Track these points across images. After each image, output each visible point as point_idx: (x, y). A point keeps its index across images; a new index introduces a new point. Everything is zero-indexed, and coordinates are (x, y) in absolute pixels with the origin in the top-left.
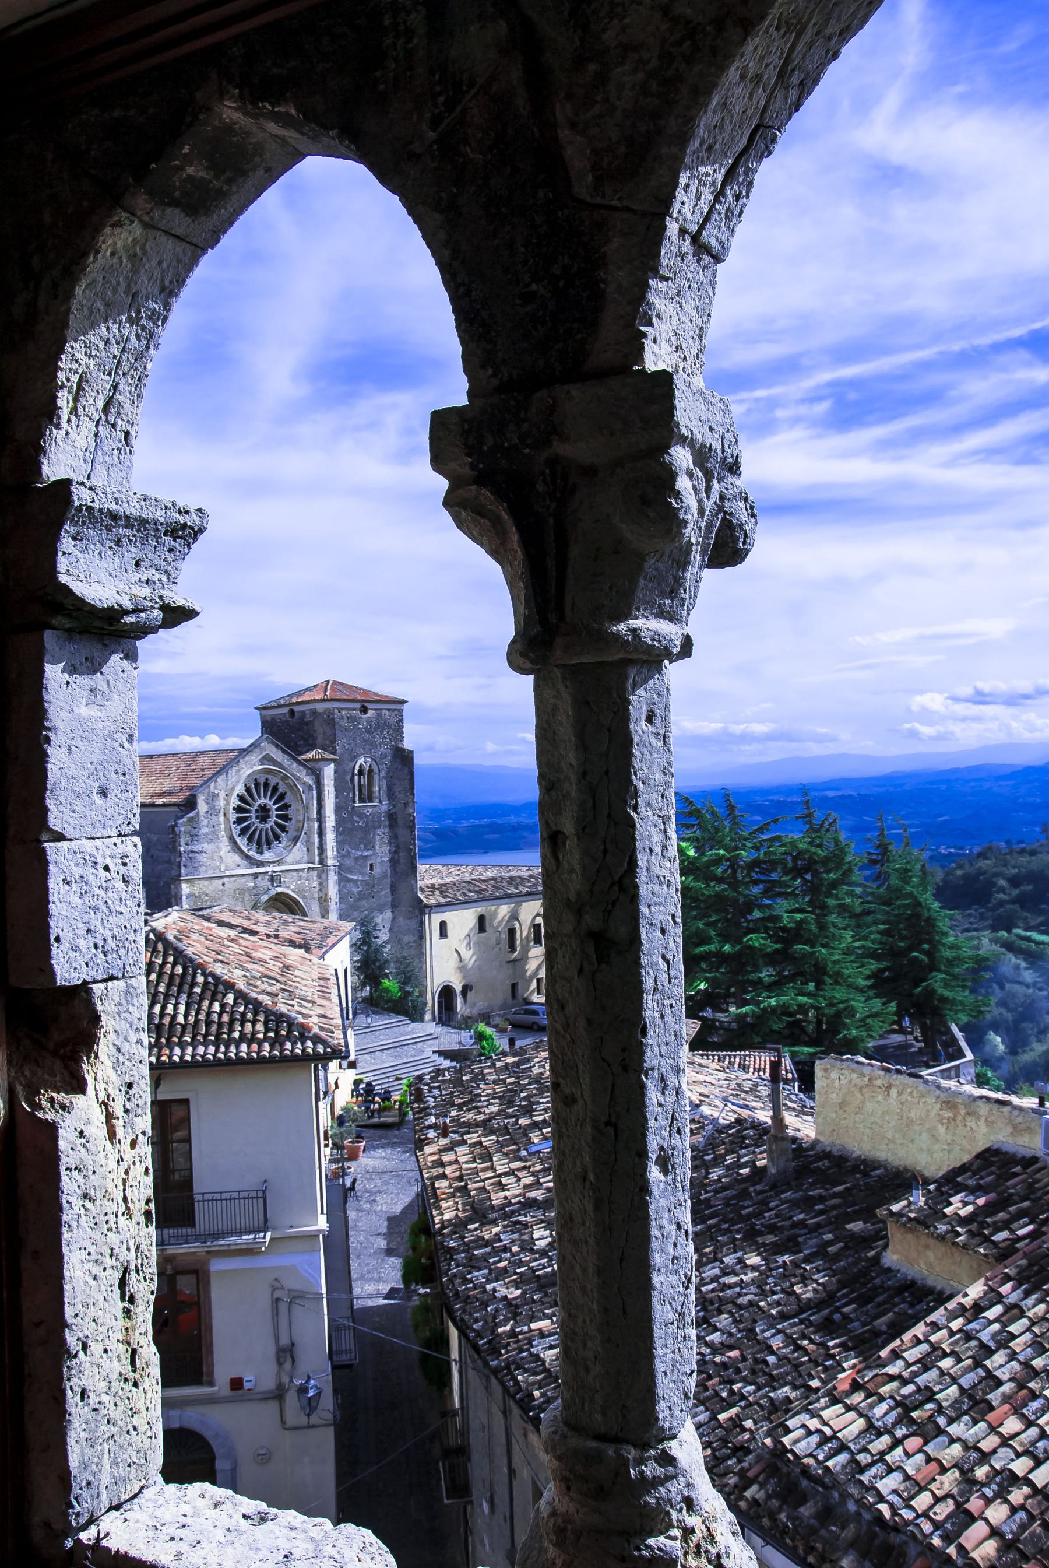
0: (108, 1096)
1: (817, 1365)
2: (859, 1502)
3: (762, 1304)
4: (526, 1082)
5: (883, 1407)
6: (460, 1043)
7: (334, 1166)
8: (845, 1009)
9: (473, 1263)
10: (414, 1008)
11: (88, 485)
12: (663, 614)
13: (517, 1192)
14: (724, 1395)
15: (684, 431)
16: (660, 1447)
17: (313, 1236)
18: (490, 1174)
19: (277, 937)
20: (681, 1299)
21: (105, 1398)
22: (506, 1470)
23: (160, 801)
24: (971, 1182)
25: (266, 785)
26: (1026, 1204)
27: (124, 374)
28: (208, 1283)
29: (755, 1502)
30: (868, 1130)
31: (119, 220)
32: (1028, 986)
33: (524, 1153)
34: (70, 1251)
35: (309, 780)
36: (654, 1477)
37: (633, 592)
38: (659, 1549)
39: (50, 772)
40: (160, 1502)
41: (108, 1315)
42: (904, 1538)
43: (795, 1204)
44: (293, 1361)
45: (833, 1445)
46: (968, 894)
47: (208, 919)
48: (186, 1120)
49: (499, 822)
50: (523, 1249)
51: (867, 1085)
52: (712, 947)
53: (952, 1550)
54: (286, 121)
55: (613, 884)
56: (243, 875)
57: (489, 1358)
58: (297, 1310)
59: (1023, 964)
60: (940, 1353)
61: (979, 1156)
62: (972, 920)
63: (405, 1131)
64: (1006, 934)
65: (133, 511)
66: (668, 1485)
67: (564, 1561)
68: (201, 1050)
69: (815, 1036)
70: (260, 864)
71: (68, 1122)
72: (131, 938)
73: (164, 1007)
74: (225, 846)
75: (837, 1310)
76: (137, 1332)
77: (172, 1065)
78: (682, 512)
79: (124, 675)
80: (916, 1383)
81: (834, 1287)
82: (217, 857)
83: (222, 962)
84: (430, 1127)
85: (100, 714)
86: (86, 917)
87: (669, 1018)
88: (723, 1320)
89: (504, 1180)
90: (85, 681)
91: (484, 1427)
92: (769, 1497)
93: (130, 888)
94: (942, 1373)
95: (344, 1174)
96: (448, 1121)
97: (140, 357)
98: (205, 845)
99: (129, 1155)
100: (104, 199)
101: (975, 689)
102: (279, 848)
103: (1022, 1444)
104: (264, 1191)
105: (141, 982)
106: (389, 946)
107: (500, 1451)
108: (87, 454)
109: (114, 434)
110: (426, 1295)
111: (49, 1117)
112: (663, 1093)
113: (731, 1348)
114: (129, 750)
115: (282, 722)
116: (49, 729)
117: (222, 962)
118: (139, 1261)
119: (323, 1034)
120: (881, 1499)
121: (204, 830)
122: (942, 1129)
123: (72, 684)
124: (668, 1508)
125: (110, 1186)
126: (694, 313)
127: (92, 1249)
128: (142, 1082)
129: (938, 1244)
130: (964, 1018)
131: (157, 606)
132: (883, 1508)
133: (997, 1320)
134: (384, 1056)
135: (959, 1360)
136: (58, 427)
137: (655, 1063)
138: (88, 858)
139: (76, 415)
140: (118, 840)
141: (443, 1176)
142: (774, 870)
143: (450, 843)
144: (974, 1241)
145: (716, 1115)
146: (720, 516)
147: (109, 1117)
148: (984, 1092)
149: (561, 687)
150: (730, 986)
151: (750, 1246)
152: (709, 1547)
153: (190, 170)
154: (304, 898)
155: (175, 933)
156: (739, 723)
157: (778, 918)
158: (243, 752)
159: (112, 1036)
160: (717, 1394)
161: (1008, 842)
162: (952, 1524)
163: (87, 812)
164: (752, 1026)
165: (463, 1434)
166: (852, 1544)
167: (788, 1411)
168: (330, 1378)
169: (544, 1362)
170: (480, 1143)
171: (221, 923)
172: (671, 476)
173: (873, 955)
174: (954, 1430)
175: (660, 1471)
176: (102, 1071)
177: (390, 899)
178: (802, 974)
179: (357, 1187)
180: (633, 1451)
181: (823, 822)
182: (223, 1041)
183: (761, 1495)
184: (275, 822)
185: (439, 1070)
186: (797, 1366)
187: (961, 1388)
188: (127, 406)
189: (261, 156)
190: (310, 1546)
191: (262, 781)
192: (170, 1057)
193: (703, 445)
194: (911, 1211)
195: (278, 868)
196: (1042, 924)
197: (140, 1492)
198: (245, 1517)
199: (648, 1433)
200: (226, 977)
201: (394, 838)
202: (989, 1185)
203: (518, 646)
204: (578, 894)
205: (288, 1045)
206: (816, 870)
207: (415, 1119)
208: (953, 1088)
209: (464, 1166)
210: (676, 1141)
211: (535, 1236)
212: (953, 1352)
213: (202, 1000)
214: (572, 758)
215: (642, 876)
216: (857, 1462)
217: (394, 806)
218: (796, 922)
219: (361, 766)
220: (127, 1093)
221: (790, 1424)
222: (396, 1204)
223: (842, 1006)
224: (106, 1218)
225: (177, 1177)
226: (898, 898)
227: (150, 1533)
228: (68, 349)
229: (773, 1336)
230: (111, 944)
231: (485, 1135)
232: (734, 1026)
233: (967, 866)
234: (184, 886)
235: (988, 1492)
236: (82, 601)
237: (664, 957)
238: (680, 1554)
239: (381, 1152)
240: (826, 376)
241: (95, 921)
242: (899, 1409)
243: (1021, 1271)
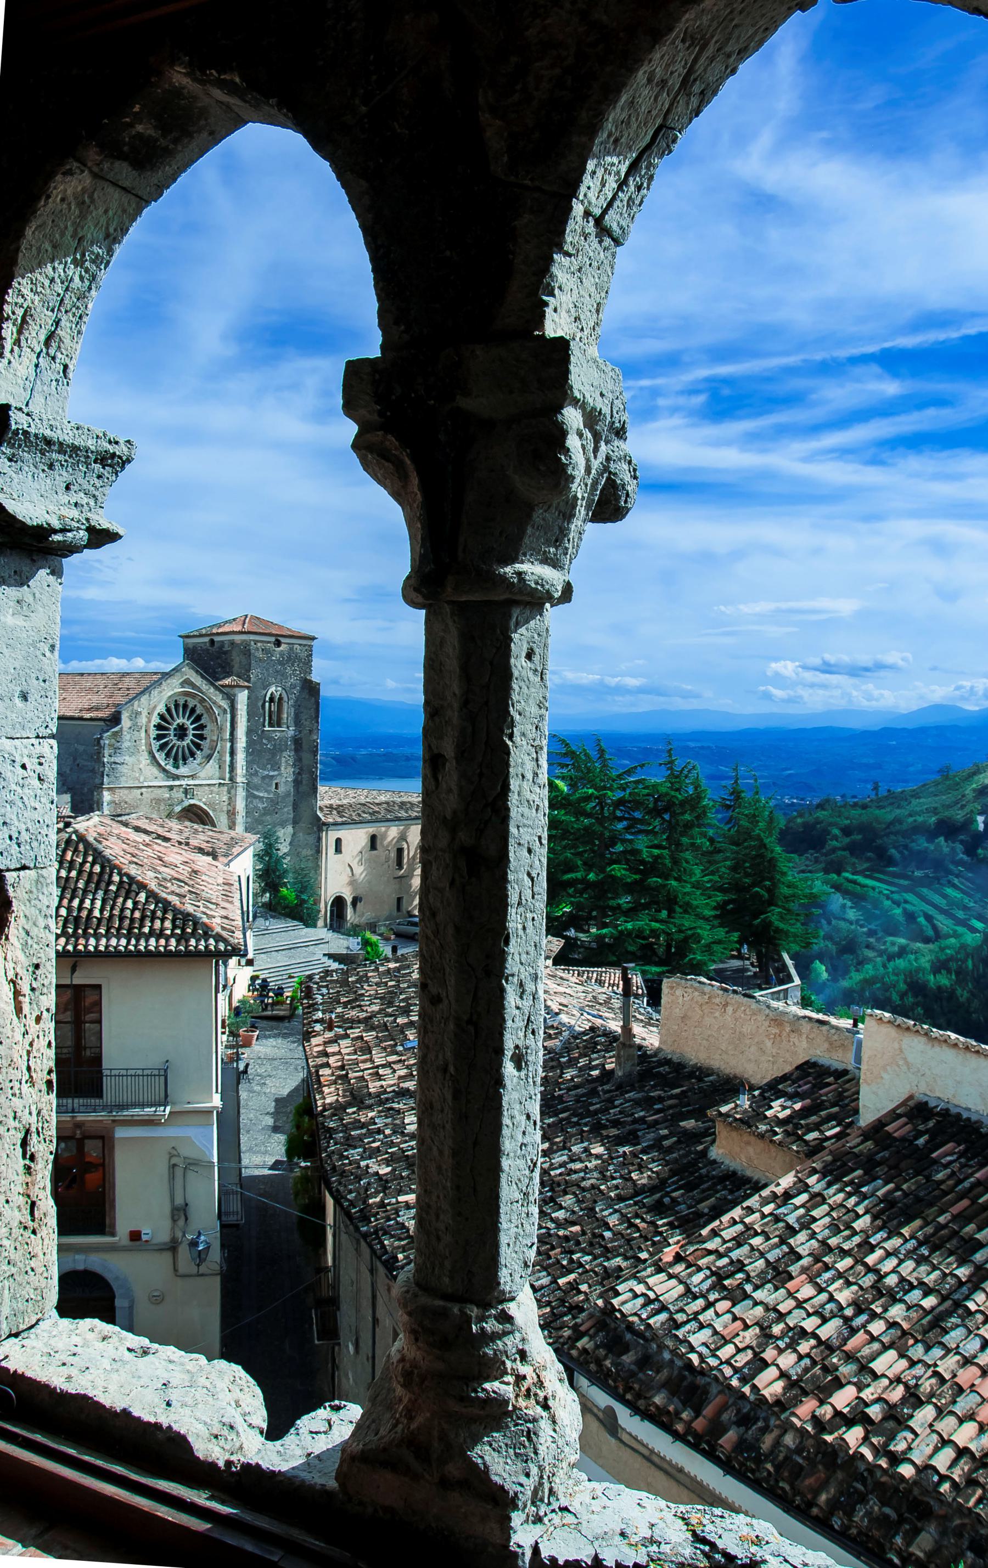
1: (646, 1239)
2: (674, 1352)
3: (602, 1187)
4: (406, 985)
5: (701, 1276)
7: (230, 1051)
9: (350, 1142)
11: (26, 410)
12: (547, 561)
13: (392, 1082)
14: (565, 1263)
15: (577, 394)
17: (209, 1112)
18: (368, 1065)
19: (187, 844)
23: (88, 716)
24: (790, 1090)
26: (836, 1109)
29: (585, 1351)
32: (851, 923)
33: (400, 1048)
35: (225, 704)
37: (521, 539)
43: (637, 1103)
44: (186, 1219)
45: (656, 1306)
47: (126, 824)
48: (99, 1003)
49: (395, 751)
52: (579, 875)
53: (747, 1390)
59: (849, 904)
61: (797, 1068)
63: (295, 1023)
65: (67, 438)
66: (505, 1339)
68: (114, 942)
70: (176, 777)
72: (44, 832)
74: (144, 759)
77: (87, 954)
78: (570, 468)
79: (49, 589)
81: (666, 1175)
82: (135, 767)
84: (317, 1021)
88: (568, 1200)
89: (381, 1071)
92: (597, 1347)
93: (45, 786)
95: (238, 1059)
97: (82, 297)
98: (127, 758)
103: (813, 1306)
104: (166, 1071)
105: (51, 873)
109: (53, 366)
110: (307, 1167)
112: (521, 998)
113: (574, 1223)
115: (202, 650)
119: (224, 934)
120: (692, 1349)
122: (769, 1044)
124: (504, 1358)
125: (16, 1057)
126: (593, 289)
128: (48, 964)
132: (694, 1358)
133: (803, 1206)
134: (279, 956)
135: (768, 1238)
137: (515, 970)
139: (19, 346)
140: (36, 741)
141: (327, 1065)
143: (348, 768)
144: (789, 1140)
145: (573, 1022)
147: (17, 993)
149: (450, 623)
150: (592, 910)
153: (140, 128)
154: (214, 810)
155: (95, 835)
156: (613, 676)
158: (166, 675)
159: (22, 921)
160: (558, 1262)
161: (843, 796)
163: (9, 714)
165: (334, 1288)
167: (618, 1277)
168: (218, 1235)
170: (361, 1038)
171: (137, 829)
172: (562, 434)
173: (721, 889)
174: (758, 1295)
175: (499, 1327)
178: (657, 903)
179: (249, 1071)
180: (475, 1310)
186: (629, 1241)
187: (767, 1261)
188: (67, 340)
191: (181, 702)
192: (86, 946)
193: (594, 409)
195: (191, 782)
201: (298, 761)
203: (412, 581)
204: (455, 812)
205: (193, 942)
210: (530, 1041)
211: (406, 1121)
212: (763, 1232)
213: (116, 897)
215: (513, 799)
216: (674, 1321)
221: (620, 1288)
223: (690, 932)
225: (88, 1053)
228: (15, 284)
230: (25, 836)
231: (366, 1031)
232: (594, 945)
233: (807, 815)
234: (106, 793)
235: (782, 1344)
236: (13, 518)
237: (529, 874)
241: (11, 815)
242: (714, 1278)
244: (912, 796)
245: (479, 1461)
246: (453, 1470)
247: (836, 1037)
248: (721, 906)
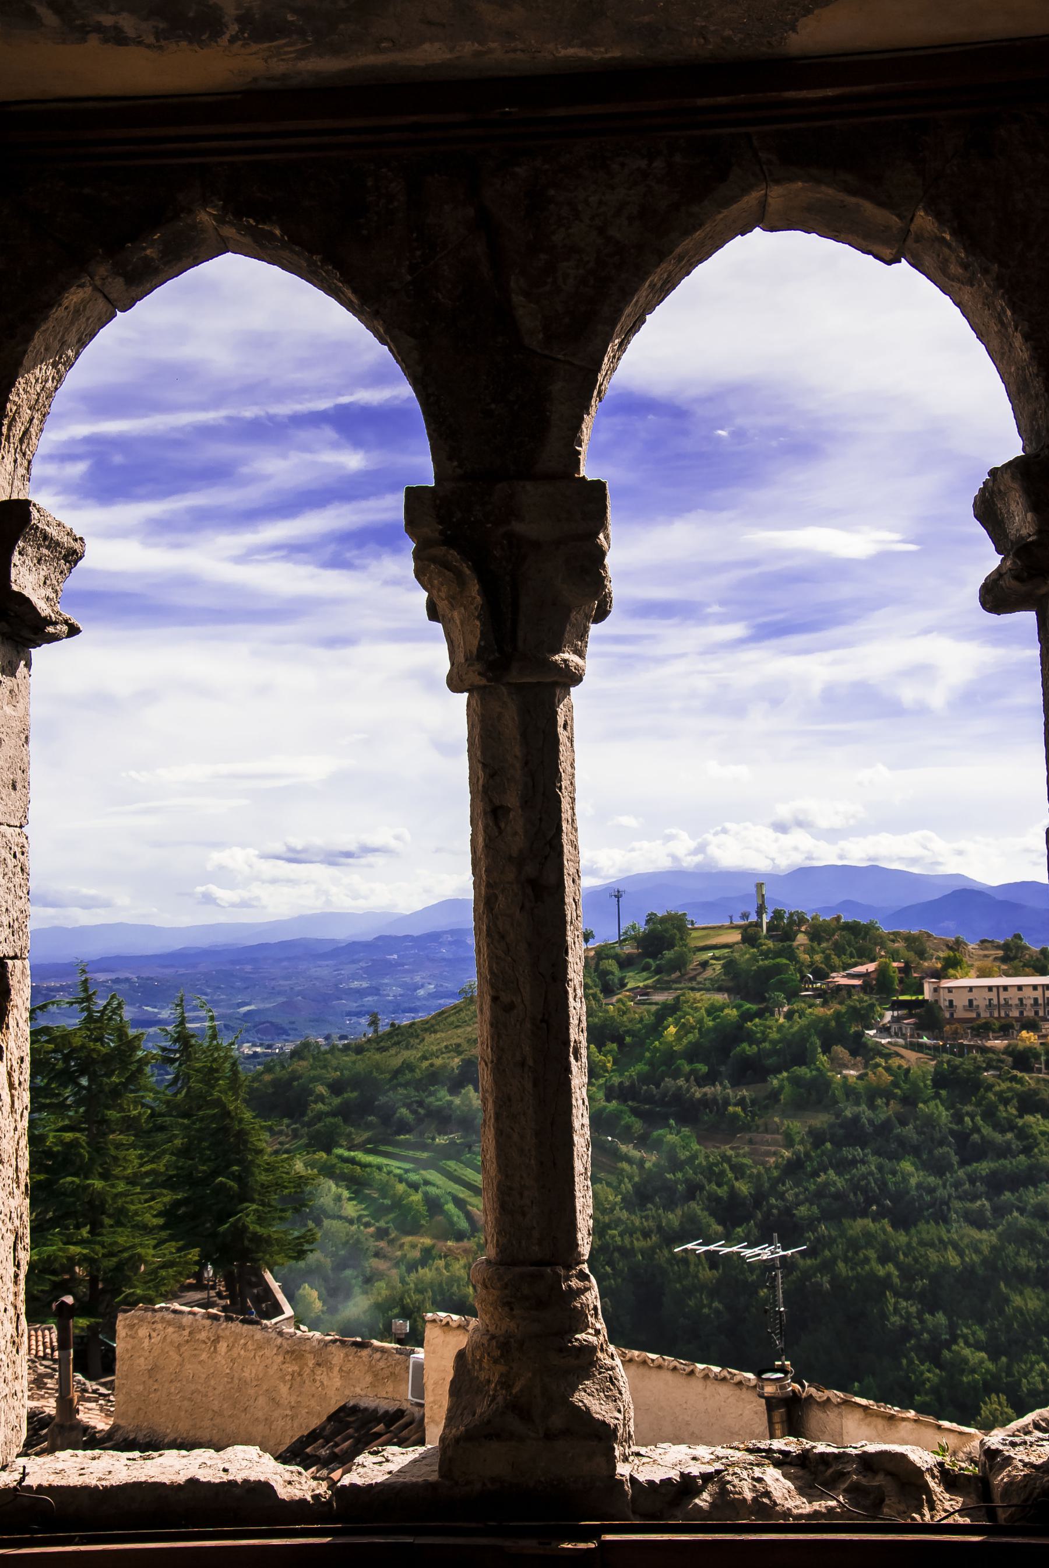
8: (131, 1257)
24: (323, 1452)
30: (186, 1403)
32: (351, 1222)
37: (563, 634)
51: (187, 1341)
59: (346, 1194)
61: (330, 1418)
62: (282, 1139)
64: (324, 1155)
69: (87, 1299)
101: (285, 844)
122: (284, 1389)
173: (169, 1183)
175: (581, 1284)
181: (105, 1007)
196: (369, 1141)
206: (95, 1071)
214: (517, 750)
223: (126, 1255)
226: (199, 1109)
240: (82, 430)
244: (426, 1030)
245: (581, 1404)
246: (557, 1422)
247: (382, 1364)
248: (169, 1214)
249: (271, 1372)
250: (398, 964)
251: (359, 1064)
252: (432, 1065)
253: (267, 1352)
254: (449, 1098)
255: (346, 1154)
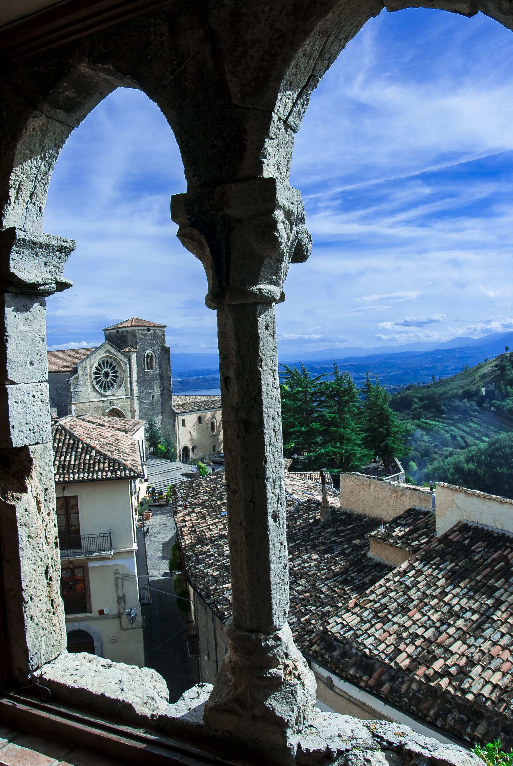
0: (37, 494)
1: (341, 597)
2: (357, 649)
3: (318, 574)
4: (220, 486)
5: (367, 612)
6: (191, 470)
7: (139, 523)
8: (353, 453)
10: (172, 456)
11: (23, 229)
12: (272, 283)
13: (216, 532)
14: (303, 611)
16: (274, 634)
17: (131, 552)
19: (113, 427)
20: (283, 574)
21: (41, 619)
22: (214, 643)
23: (62, 370)
24: (403, 522)
25: (107, 362)
26: (425, 530)
27: (39, 182)
28: (88, 571)
29: (315, 651)
31: (36, 115)
34: (23, 559)
35: (126, 360)
36: (272, 646)
38: (274, 673)
39: (8, 354)
40: (66, 660)
41: (40, 586)
42: (374, 661)
44: (125, 603)
45: (347, 628)
46: (402, 404)
47: (83, 420)
48: (76, 505)
49: (207, 377)
50: (219, 555)
52: (297, 429)
53: (392, 664)
54: (108, 72)
55: (251, 399)
56: (98, 401)
57: (206, 599)
58: (125, 582)
59: (425, 433)
60: (390, 590)
61: (406, 512)
63: (169, 507)
65: (43, 241)
66: (278, 648)
67: (235, 680)
68: (82, 475)
70: (106, 396)
71: (20, 505)
72: (45, 426)
73: (65, 458)
74: (90, 389)
75: (349, 575)
76: (54, 592)
77: (70, 482)
78: (280, 239)
80: (380, 603)
82: (86, 393)
83: (90, 438)
84: (179, 506)
85: (29, 329)
86: (25, 418)
87: (276, 456)
88: (303, 581)
89: (211, 527)
90: (23, 315)
91: (204, 627)
92: (321, 649)
94: (391, 598)
95: (144, 526)
96: (187, 503)
98: (82, 389)
99: (47, 518)
100: (30, 106)
101: (404, 319)
102: (113, 390)
103: (421, 623)
104: (110, 534)
106: (161, 430)
107: (211, 636)
108: (23, 216)
111: (12, 503)
112: (274, 488)
113: (306, 592)
114: (42, 345)
115: (113, 336)
116: (7, 336)
117: (90, 438)
118: (53, 563)
119: (133, 468)
120: (366, 647)
121: (81, 382)
122: (391, 501)
123: (17, 316)
124: (278, 657)
127: (33, 558)
129: (390, 547)
130: (401, 456)
131: (54, 282)
132: (367, 651)
133: (413, 576)
135: (397, 593)
136: (10, 204)
137: (270, 475)
138: (25, 392)
139: (18, 200)
140: (38, 384)
141: (186, 526)
142: (322, 396)
143: (186, 386)
145: (299, 498)
146: (296, 241)
147: (38, 503)
148: (408, 486)
150: (305, 445)
151: (313, 551)
152: (295, 672)
153: (67, 93)
154: (124, 410)
155: (69, 426)
157: (325, 416)
158: (97, 349)
159: (38, 468)
160: (300, 610)
161: (418, 383)
162: (393, 655)
163: (25, 372)
164: (314, 461)
165: (196, 630)
166: (354, 665)
167: (329, 616)
168: (140, 609)
169: (229, 601)
170: (201, 512)
171: (89, 422)
173: (364, 431)
174: (395, 619)
176: (34, 483)
177: (161, 411)
178: (334, 439)
180: (263, 636)
182: (88, 470)
183: (318, 649)
184: (112, 379)
185: (183, 482)
186: (332, 598)
187: (398, 603)
188: (40, 195)
189: (98, 87)
190: (130, 677)
191: (105, 361)
192: (69, 478)
193: (289, 210)
194: (379, 535)
196: (432, 417)
197: (58, 656)
198: (102, 665)
199: (269, 628)
200: (91, 444)
201: (162, 384)
202: (410, 523)
203: (210, 297)
205: (119, 473)
207: (173, 503)
208: (396, 485)
209: (194, 522)
210: (280, 508)
211: (224, 550)
212: (395, 590)
213: (81, 454)
215: (264, 395)
216: (356, 634)
217: (162, 371)
218: (331, 418)
219: (148, 354)
220: (45, 492)
222: (166, 538)
223: (351, 452)
224: (38, 545)
226: (374, 407)
227: (63, 673)
228: (14, 170)
229: (323, 586)
230: (37, 429)
232: (306, 461)
233: (402, 393)
234: (73, 406)
235: (407, 642)
236: (21, 280)
237: (274, 430)
238: (283, 675)
239: (159, 517)
240: (339, 189)
241: (29, 419)
242: (374, 613)
243: (423, 556)
244: (451, 381)
245: (270, 706)
249: (387, 496)
250: (441, 359)
251: (429, 392)
252: (453, 392)
253: (386, 490)
254: (459, 403)
255: (424, 421)
